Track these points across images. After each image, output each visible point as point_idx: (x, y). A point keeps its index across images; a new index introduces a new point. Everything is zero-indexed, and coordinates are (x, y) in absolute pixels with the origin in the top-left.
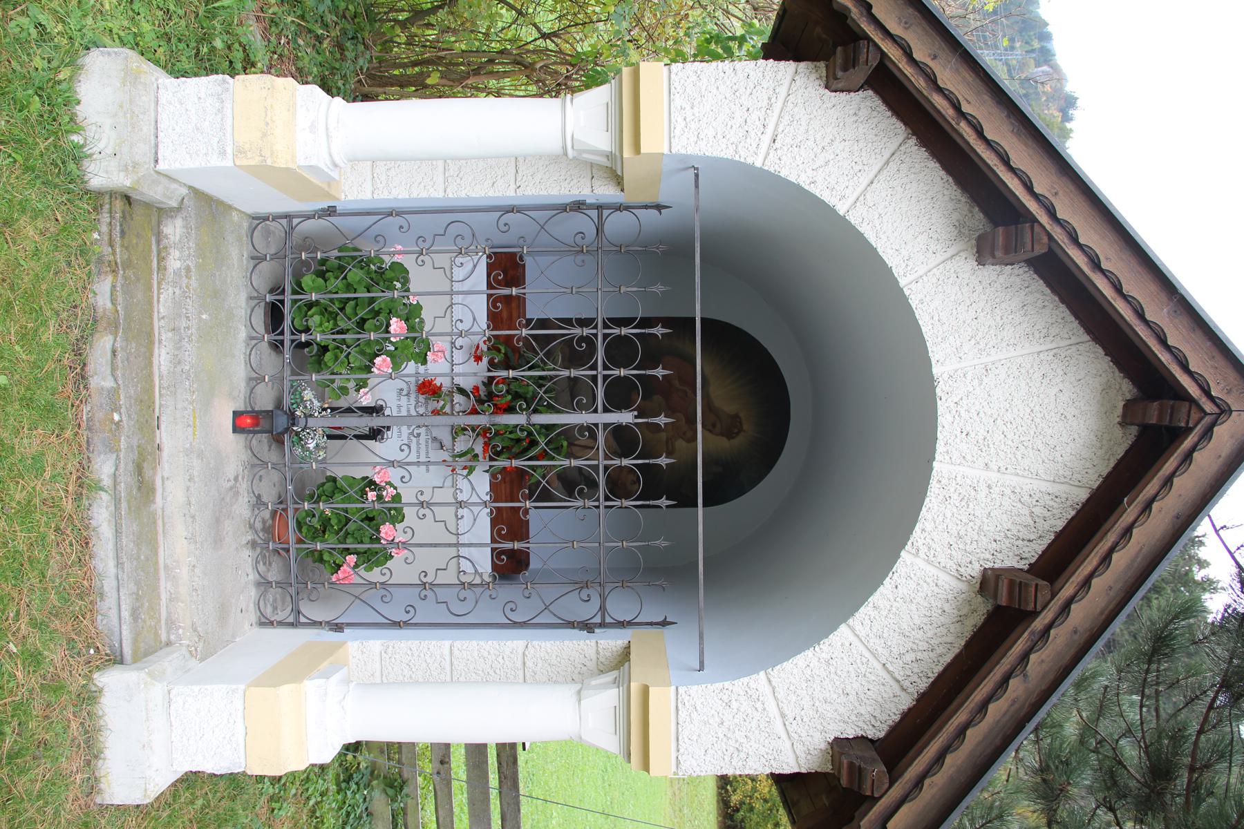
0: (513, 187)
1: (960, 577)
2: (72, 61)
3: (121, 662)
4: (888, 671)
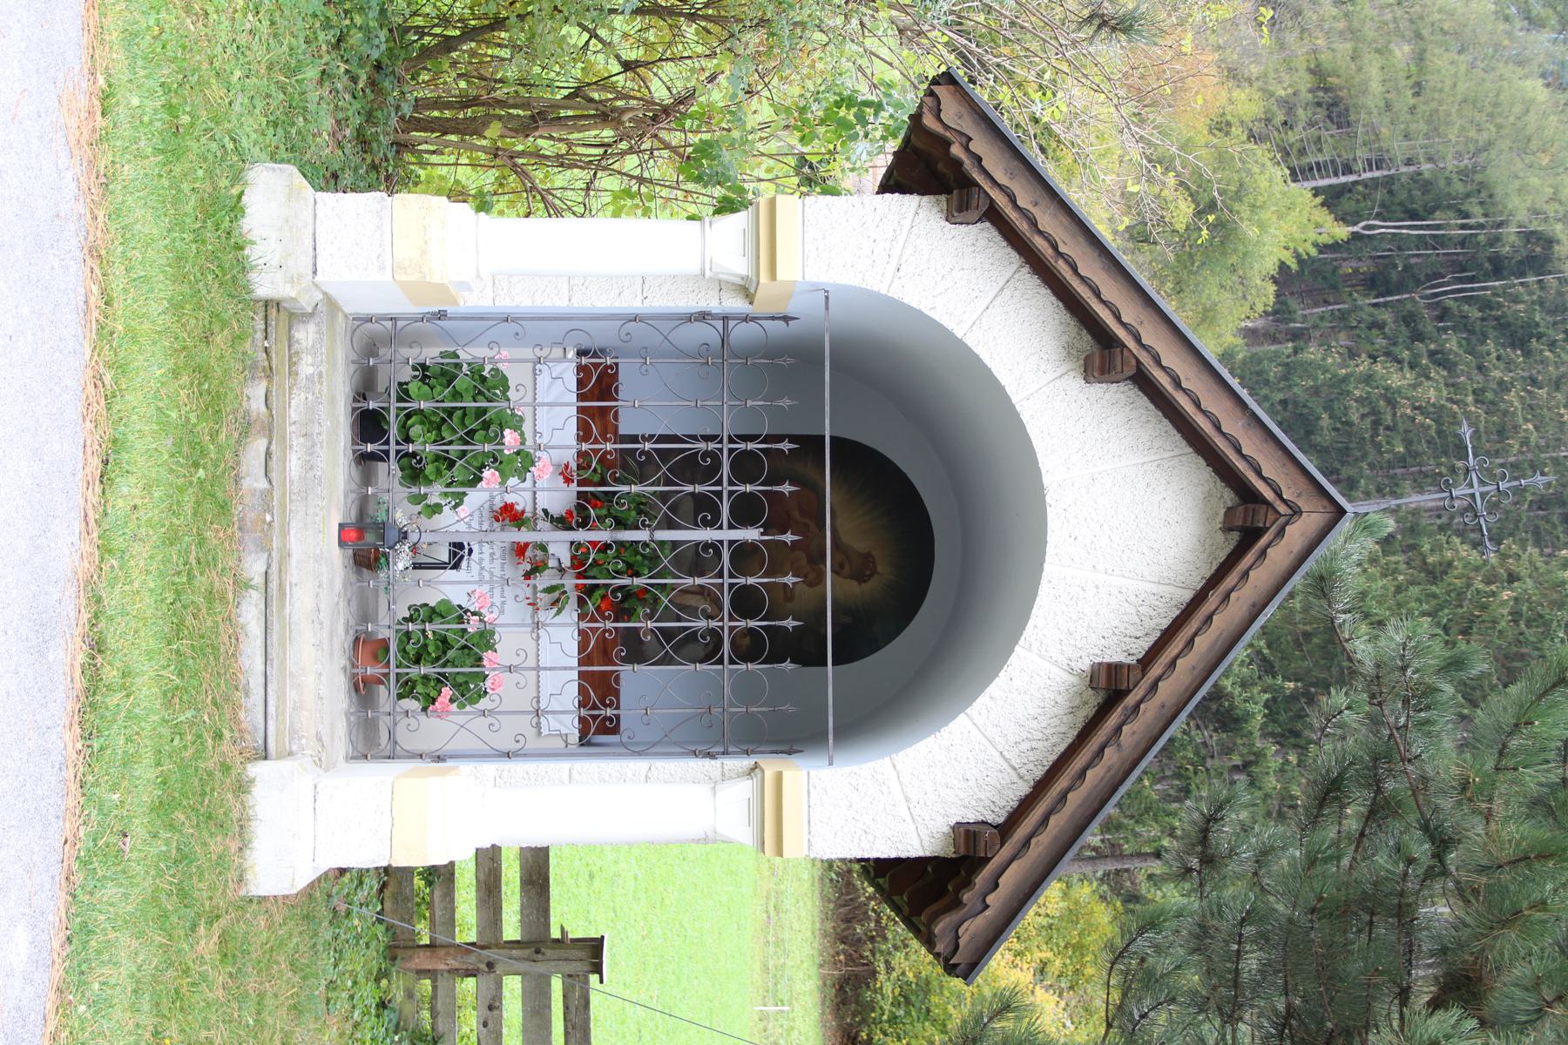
0: (640, 297)
1: (1071, 671)
2: (237, 177)
3: (266, 758)
4: (1006, 759)
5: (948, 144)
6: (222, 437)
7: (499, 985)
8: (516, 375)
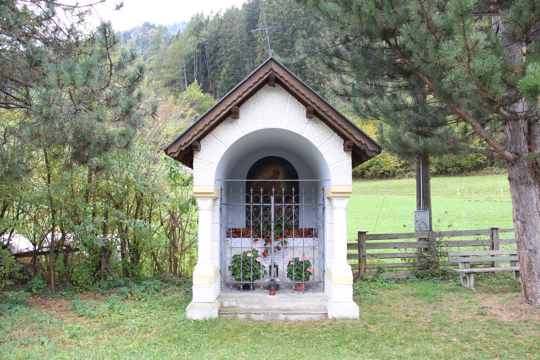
1: (308, 123)
2: (189, 321)
3: (327, 314)
5: (182, 151)
6: (252, 325)
7: (368, 254)
8: (234, 253)
